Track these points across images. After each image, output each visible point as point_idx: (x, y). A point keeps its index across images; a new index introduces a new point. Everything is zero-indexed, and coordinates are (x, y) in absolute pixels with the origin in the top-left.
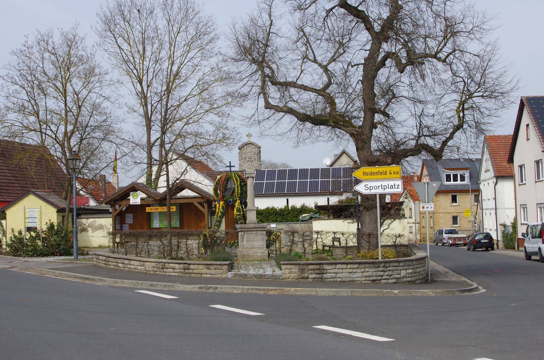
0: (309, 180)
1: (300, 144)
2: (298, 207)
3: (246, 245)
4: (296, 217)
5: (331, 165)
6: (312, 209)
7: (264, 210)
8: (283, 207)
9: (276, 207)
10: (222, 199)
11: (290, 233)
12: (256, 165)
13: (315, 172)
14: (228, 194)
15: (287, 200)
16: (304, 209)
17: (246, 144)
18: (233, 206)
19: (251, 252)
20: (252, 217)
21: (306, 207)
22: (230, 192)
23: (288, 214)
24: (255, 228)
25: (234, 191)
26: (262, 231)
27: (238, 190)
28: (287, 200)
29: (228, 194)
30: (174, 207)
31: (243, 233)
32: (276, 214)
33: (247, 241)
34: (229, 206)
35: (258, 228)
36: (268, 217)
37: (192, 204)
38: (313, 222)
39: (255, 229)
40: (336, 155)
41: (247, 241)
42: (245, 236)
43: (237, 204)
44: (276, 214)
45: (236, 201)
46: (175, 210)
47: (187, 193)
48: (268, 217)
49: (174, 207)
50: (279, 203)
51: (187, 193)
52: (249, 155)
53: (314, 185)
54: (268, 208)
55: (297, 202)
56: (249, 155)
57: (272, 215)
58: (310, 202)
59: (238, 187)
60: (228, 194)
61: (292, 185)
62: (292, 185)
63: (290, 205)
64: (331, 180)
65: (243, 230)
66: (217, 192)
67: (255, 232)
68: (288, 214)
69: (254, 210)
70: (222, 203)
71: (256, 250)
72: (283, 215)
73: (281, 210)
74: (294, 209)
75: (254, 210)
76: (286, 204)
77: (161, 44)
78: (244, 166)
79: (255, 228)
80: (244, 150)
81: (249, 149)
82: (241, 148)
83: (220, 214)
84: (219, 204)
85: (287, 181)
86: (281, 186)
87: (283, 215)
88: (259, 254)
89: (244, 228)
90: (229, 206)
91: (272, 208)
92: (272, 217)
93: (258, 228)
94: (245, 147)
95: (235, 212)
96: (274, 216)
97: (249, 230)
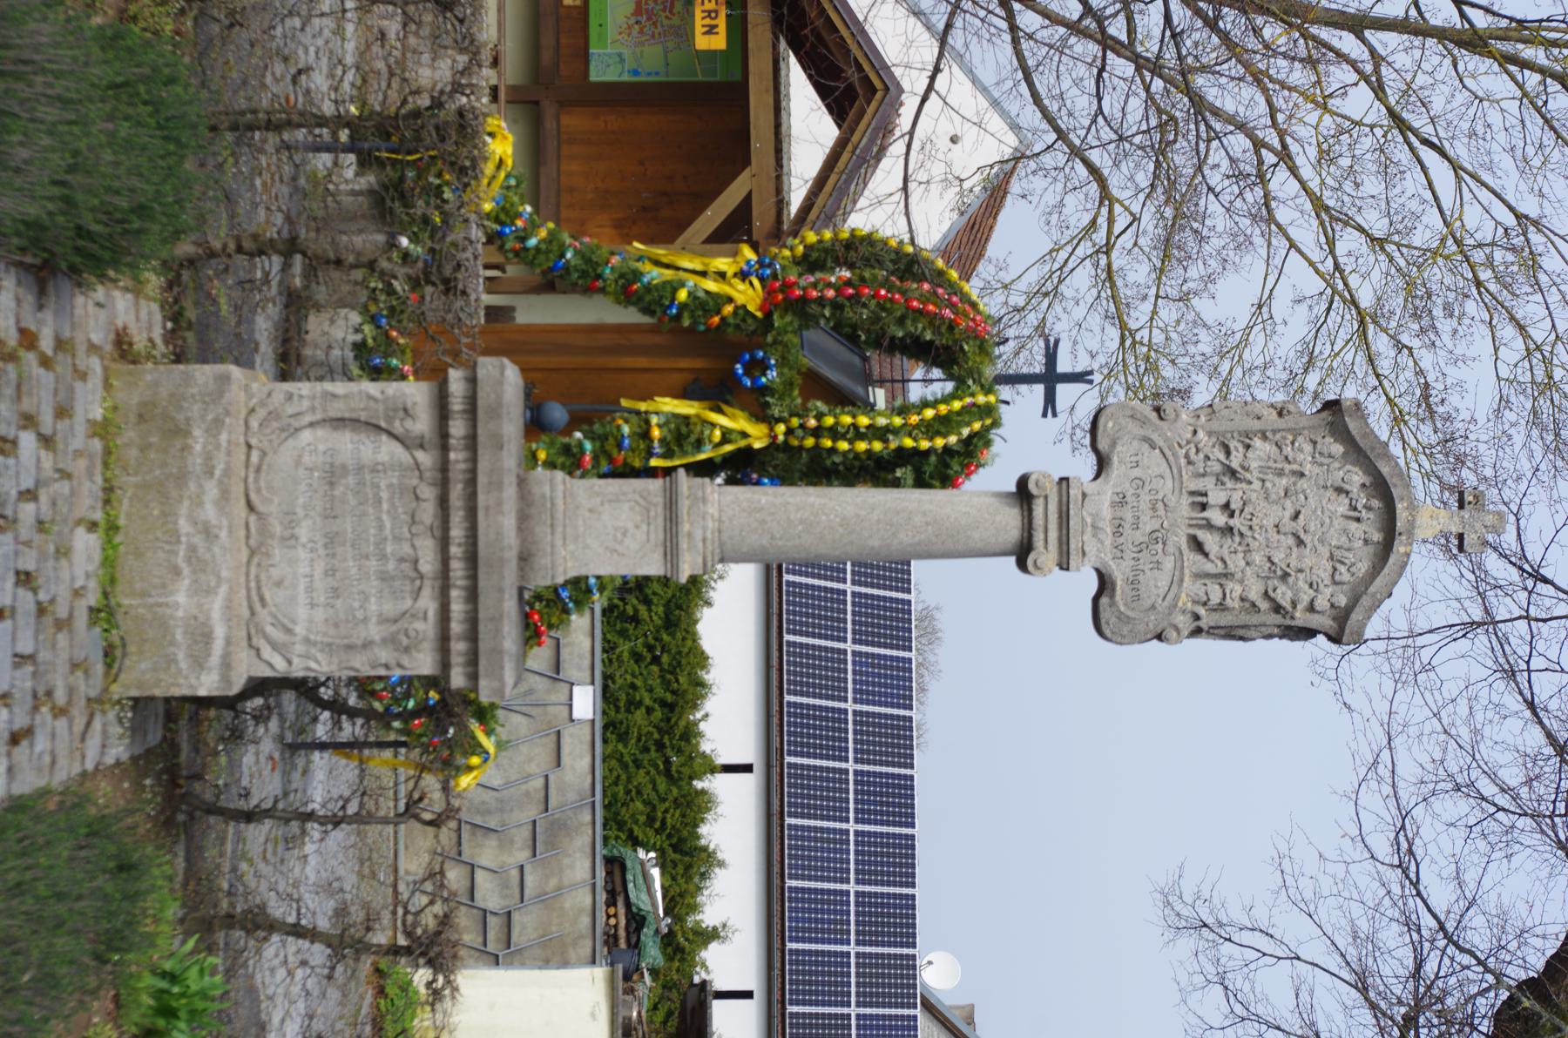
0: (852, 887)
1: (1187, 943)
2: (703, 830)
3: (284, 456)
4: (651, 820)
5: (928, 1006)
6: (694, 908)
7: (694, 638)
8: (705, 747)
9: (710, 705)
10: (781, 299)
11: (429, 921)
12: (1156, 583)
13: (894, 921)
14: (817, 351)
15: (747, 768)
16: (689, 862)
17: (1381, 489)
18: (718, 392)
19: (206, 506)
20: (604, 529)
21: (704, 876)
22: (846, 369)
23: (667, 773)
24: (472, 559)
25: (842, 399)
26: (444, 638)
27: (857, 433)
28: (747, 768)
29: (819, 349)
30: (719, 42)
31: (422, 424)
32: (671, 707)
33: (333, 474)
34: (719, 356)
35: (473, 595)
36: (656, 660)
37: (742, 159)
38: (600, 973)
39: (461, 563)
40: (970, 1021)
41: (333, 474)
42: (388, 450)
43: (736, 425)
44: (671, 707)
45: (761, 415)
46: (703, 42)
47: (810, 129)
48: (656, 660)
49: (719, 42)
50: (729, 720)
51: (810, 129)
52: (1271, 515)
53: (824, 915)
54: (702, 660)
55: (733, 822)
56: (1271, 515)
57: (666, 684)
58: (732, 899)
59: (882, 433)
60: (817, 351)
61: (824, 794)
62: (824, 794)
63: (718, 785)
64: (853, 1011)
65: (457, 428)
66: (840, 262)
67: (428, 564)
68: (667, 773)
69: (671, 551)
70: (748, 295)
71: (228, 558)
72: (660, 746)
73: (690, 734)
74: (696, 807)
75: (671, 551)
76: (722, 760)
77: (264, 858)
78: (1154, 463)
79: (472, 559)
80: (1320, 461)
81: (1336, 521)
82: (1340, 431)
83: (654, 274)
84: (743, 275)
85: (851, 766)
86: (823, 733)
87: (660, 746)
88: (182, 598)
89: (472, 442)
90: (719, 356)
91: (701, 684)
92: (655, 683)
93: (473, 595)
94: (1357, 478)
95: (670, 405)
96: (659, 692)
97: (454, 489)
